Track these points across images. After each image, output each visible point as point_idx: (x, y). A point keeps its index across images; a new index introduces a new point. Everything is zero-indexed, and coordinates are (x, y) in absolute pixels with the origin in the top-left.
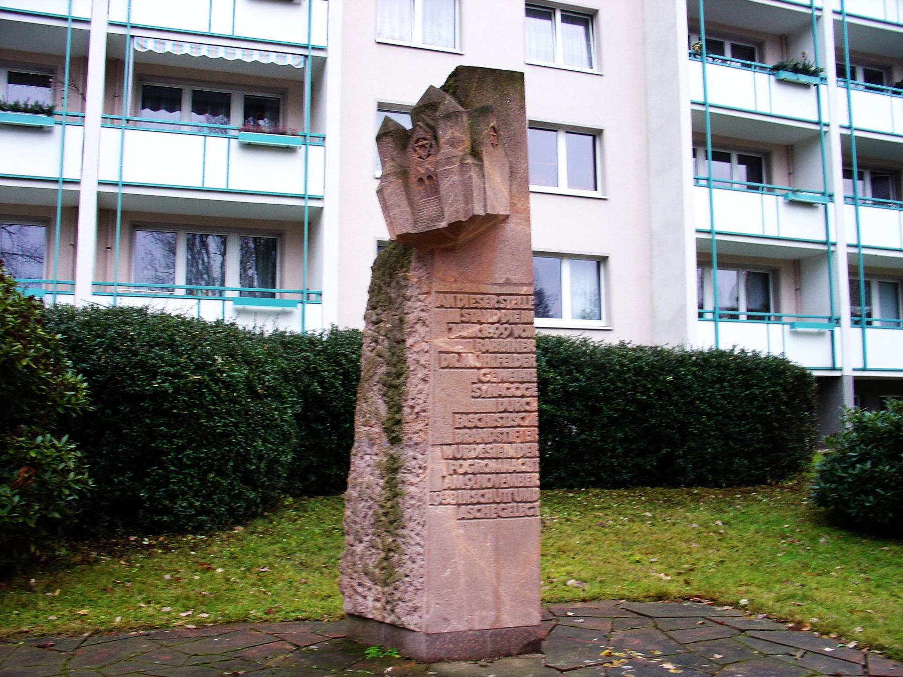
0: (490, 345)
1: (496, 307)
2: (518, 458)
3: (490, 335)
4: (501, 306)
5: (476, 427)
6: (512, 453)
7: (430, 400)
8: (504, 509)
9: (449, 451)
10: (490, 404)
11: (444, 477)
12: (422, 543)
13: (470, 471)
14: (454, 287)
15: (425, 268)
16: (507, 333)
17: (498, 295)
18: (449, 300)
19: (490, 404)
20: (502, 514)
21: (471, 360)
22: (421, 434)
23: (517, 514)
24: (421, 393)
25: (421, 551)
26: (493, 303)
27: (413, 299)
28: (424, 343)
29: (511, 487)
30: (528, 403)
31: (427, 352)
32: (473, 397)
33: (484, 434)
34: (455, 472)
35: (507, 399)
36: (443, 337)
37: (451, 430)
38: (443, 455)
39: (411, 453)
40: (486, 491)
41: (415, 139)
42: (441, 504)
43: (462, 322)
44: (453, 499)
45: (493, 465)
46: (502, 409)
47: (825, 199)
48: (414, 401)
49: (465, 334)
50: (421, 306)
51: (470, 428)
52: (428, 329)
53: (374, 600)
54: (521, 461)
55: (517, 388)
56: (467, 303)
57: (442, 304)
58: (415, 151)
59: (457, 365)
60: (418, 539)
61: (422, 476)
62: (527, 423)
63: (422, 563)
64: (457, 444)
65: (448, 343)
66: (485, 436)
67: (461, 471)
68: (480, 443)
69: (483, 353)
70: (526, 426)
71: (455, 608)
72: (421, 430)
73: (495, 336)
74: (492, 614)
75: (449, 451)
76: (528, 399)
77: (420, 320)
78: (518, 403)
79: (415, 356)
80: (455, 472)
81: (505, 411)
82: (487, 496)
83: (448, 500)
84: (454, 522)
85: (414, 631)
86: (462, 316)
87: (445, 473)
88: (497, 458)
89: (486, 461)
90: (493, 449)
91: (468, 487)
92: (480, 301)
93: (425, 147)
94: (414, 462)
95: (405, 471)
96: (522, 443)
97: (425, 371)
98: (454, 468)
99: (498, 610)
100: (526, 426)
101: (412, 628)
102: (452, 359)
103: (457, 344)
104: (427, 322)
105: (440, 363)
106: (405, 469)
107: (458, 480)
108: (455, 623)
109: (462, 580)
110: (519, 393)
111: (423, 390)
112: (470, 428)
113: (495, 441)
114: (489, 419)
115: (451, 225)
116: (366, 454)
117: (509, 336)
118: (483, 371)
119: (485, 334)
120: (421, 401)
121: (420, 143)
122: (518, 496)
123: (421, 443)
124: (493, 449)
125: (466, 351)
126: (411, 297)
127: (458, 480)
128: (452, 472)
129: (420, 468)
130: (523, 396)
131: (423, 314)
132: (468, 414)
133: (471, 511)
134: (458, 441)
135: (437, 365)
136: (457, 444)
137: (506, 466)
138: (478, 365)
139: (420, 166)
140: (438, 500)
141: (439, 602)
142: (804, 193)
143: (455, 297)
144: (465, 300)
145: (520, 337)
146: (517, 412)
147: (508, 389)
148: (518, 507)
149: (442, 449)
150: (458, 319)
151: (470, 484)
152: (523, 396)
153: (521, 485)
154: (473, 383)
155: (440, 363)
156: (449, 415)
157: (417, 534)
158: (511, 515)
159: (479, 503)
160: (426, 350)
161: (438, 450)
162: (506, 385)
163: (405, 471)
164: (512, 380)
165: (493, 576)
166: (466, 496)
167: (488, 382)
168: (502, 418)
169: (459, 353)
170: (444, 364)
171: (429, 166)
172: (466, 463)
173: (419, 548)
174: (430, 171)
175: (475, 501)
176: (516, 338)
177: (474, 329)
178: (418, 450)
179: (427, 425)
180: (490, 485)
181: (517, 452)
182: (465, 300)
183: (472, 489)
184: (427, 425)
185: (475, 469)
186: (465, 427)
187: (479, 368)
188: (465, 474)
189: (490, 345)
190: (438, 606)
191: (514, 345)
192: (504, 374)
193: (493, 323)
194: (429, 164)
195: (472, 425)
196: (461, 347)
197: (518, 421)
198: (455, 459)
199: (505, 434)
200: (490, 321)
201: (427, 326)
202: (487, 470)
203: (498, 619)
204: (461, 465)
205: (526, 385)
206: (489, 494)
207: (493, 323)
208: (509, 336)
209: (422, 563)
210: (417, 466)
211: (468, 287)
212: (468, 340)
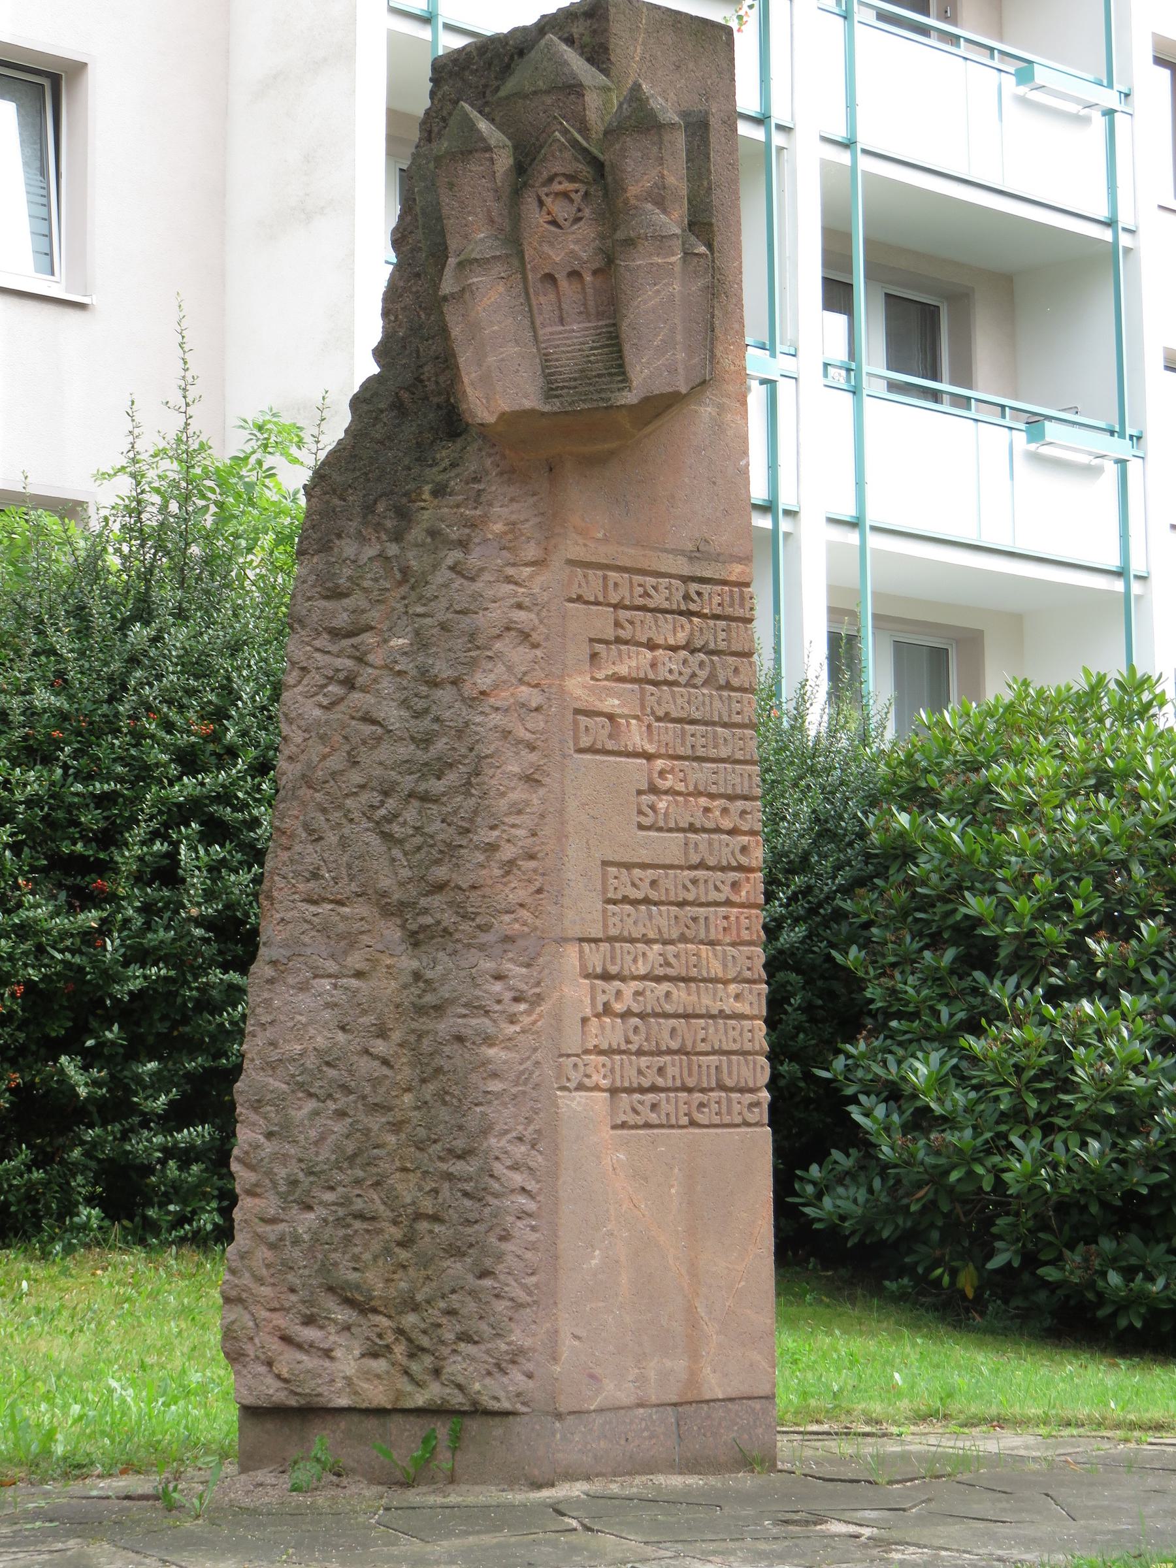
0: (675, 702)
1: (683, 607)
2: (726, 982)
3: (670, 678)
4: (693, 607)
5: (646, 901)
6: (716, 969)
7: (547, 831)
8: (702, 1105)
9: (596, 958)
10: (670, 846)
11: (585, 1020)
12: (531, 1186)
13: (636, 1008)
14: (602, 553)
15: (531, 500)
16: (703, 674)
17: (686, 579)
18: (592, 586)
19: (670, 846)
20: (700, 1118)
21: (636, 737)
22: (524, 914)
23: (727, 1119)
24: (519, 812)
25: (531, 1206)
26: (677, 602)
27: (487, 576)
28: (523, 688)
29: (714, 1052)
30: (744, 849)
31: (537, 710)
32: (641, 827)
33: (663, 919)
34: (607, 1010)
35: (705, 836)
36: (581, 673)
37: (599, 905)
38: (583, 966)
39: (489, 965)
40: (668, 1058)
41: (545, 175)
42: (581, 1087)
43: (619, 641)
44: (605, 1077)
45: (682, 996)
46: (695, 859)
47: (1120, 447)
48: (496, 833)
49: (623, 670)
50: (515, 594)
51: (635, 903)
52: (538, 653)
53: (363, 1356)
54: (733, 988)
55: (725, 811)
56: (627, 595)
57: (580, 592)
58: (541, 203)
59: (610, 745)
60: (518, 1179)
61: (526, 1020)
62: (743, 896)
63: (533, 1237)
64: (611, 939)
65: (591, 689)
66: (663, 923)
67: (619, 1007)
68: (655, 941)
69: (659, 719)
70: (742, 905)
71: (611, 1348)
72: (521, 905)
73: (683, 680)
74: (679, 1365)
75: (596, 958)
76: (745, 839)
77: (508, 629)
78: (726, 849)
79: (496, 719)
80: (607, 1010)
81: (702, 865)
82: (670, 1071)
83: (597, 1078)
84: (607, 1133)
85: (506, 1414)
86: (617, 624)
87: (588, 1011)
88: (686, 980)
89: (666, 986)
90: (683, 956)
91: (633, 1048)
92: (652, 592)
93: (572, 201)
94: (498, 987)
95: (464, 1011)
96: (733, 944)
97: (533, 757)
98: (605, 998)
99: (694, 1355)
100: (742, 905)
101: (506, 1405)
102: (599, 730)
103: (610, 693)
104: (535, 637)
105: (576, 739)
106: (465, 1006)
107: (612, 1032)
108: (612, 1386)
109: (624, 1280)
110: (727, 824)
111: (527, 803)
112: (635, 903)
113: (683, 939)
114: (672, 884)
115: (646, 400)
116: (316, 976)
117: (706, 683)
118: (659, 763)
119: (663, 674)
120: (521, 833)
121: (556, 187)
122: (730, 1073)
123: (524, 936)
124: (683, 956)
125: (626, 712)
126: (482, 570)
127: (612, 1032)
128: (600, 1008)
129: (516, 1000)
130: (732, 832)
131: (520, 616)
132: (629, 866)
133: (639, 1108)
134: (613, 932)
135: (571, 744)
136: (611, 939)
137: (707, 1001)
138: (651, 749)
139: (551, 244)
140: (575, 1076)
141: (578, 1332)
142: (1102, 425)
143: (605, 578)
144: (624, 588)
145: (728, 686)
146: (723, 869)
147: (707, 810)
148: (729, 1100)
149: (581, 952)
150: (610, 634)
151: (637, 1041)
152: (732, 832)
153: (735, 1047)
154: (640, 793)
155: (576, 739)
156: (597, 872)
157: (515, 1167)
158: (716, 1120)
159: (654, 1089)
160: (534, 705)
161: (572, 952)
162: (703, 801)
163: (464, 1011)
164: (713, 789)
165: (683, 1271)
166: (629, 1070)
167: (666, 792)
168: (694, 882)
169: (611, 717)
170: (585, 742)
171: (576, 248)
172: (629, 988)
173: (522, 1200)
174: (578, 258)
175: (646, 1083)
176: (720, 688)
177: (636, 661)
178: (510, 955)
179: (539, 891)
180: (674, 1045)
181: (725, 966)
182: (624, 588)
183: (640, 1053)
184: (539, 891)
185: (649, 1003)
186: (625, 900)
187: (649, 757)
188: (627, 1014)
189: (675, 702)
190: (576, 1343)
191: (717, 704)
192: (700, 774)
193: (674, 649)
194: (577, 242)
195: (640, 895)
196: (617, 702)
197: (726, 892)
198: (606, 977)
199: (702, 921)
200: (671, 642)
201: (535, 646)
202: (669, 1009)
203: (693, 1379)
204: (619, 993)
205: (740, 804)
206: (674, 1067)
207: (674, 649)
208: (706, 683)
209: (533, 1237)
210: (508, 995)
211: (629, 555)
212: (629, 686)
